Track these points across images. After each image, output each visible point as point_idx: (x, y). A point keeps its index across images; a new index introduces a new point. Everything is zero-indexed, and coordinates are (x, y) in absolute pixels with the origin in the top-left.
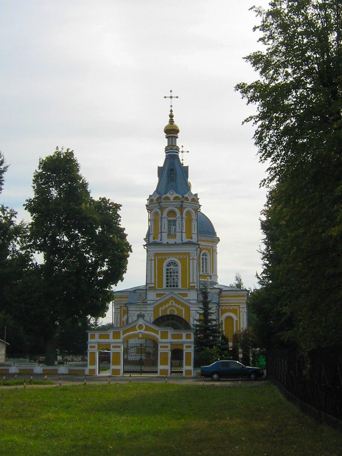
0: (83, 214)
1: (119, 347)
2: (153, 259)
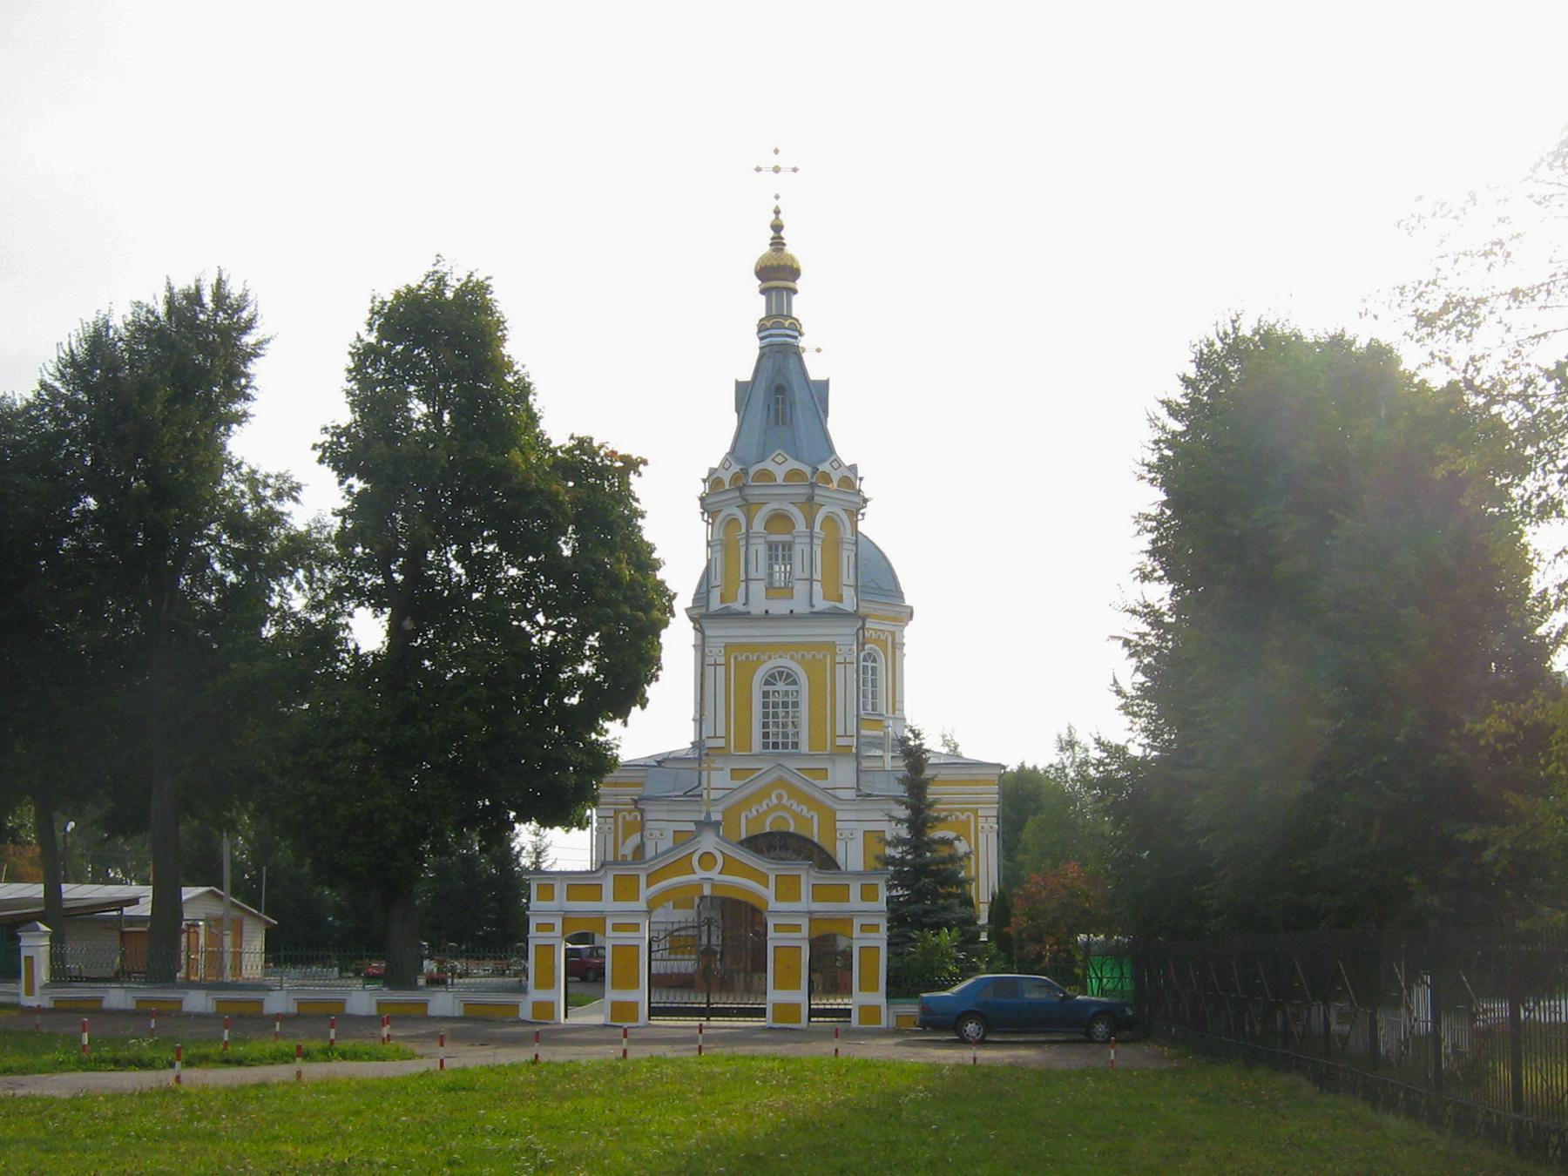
0: (515, 481)
1: (635, 927)
2: (721, 660)
